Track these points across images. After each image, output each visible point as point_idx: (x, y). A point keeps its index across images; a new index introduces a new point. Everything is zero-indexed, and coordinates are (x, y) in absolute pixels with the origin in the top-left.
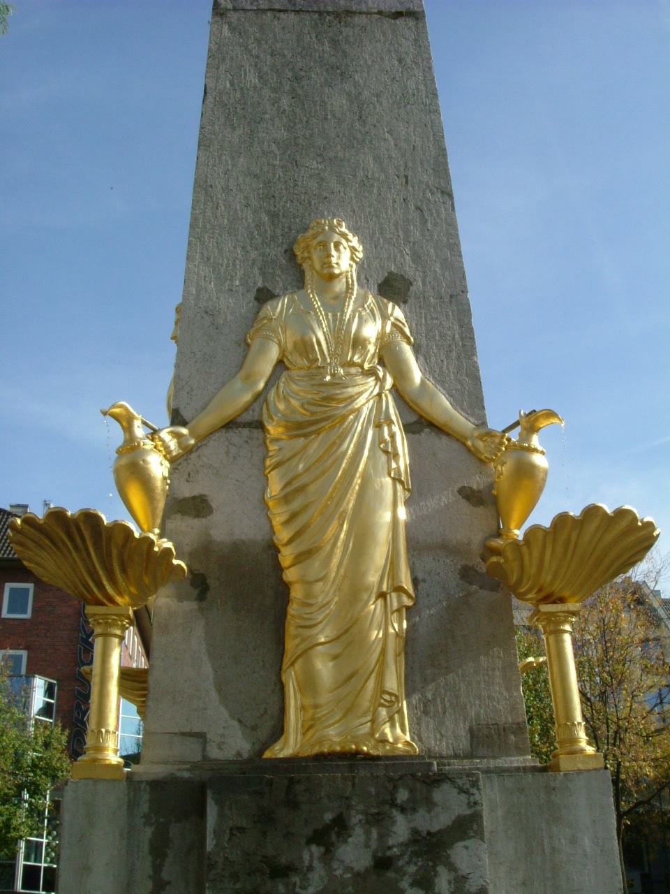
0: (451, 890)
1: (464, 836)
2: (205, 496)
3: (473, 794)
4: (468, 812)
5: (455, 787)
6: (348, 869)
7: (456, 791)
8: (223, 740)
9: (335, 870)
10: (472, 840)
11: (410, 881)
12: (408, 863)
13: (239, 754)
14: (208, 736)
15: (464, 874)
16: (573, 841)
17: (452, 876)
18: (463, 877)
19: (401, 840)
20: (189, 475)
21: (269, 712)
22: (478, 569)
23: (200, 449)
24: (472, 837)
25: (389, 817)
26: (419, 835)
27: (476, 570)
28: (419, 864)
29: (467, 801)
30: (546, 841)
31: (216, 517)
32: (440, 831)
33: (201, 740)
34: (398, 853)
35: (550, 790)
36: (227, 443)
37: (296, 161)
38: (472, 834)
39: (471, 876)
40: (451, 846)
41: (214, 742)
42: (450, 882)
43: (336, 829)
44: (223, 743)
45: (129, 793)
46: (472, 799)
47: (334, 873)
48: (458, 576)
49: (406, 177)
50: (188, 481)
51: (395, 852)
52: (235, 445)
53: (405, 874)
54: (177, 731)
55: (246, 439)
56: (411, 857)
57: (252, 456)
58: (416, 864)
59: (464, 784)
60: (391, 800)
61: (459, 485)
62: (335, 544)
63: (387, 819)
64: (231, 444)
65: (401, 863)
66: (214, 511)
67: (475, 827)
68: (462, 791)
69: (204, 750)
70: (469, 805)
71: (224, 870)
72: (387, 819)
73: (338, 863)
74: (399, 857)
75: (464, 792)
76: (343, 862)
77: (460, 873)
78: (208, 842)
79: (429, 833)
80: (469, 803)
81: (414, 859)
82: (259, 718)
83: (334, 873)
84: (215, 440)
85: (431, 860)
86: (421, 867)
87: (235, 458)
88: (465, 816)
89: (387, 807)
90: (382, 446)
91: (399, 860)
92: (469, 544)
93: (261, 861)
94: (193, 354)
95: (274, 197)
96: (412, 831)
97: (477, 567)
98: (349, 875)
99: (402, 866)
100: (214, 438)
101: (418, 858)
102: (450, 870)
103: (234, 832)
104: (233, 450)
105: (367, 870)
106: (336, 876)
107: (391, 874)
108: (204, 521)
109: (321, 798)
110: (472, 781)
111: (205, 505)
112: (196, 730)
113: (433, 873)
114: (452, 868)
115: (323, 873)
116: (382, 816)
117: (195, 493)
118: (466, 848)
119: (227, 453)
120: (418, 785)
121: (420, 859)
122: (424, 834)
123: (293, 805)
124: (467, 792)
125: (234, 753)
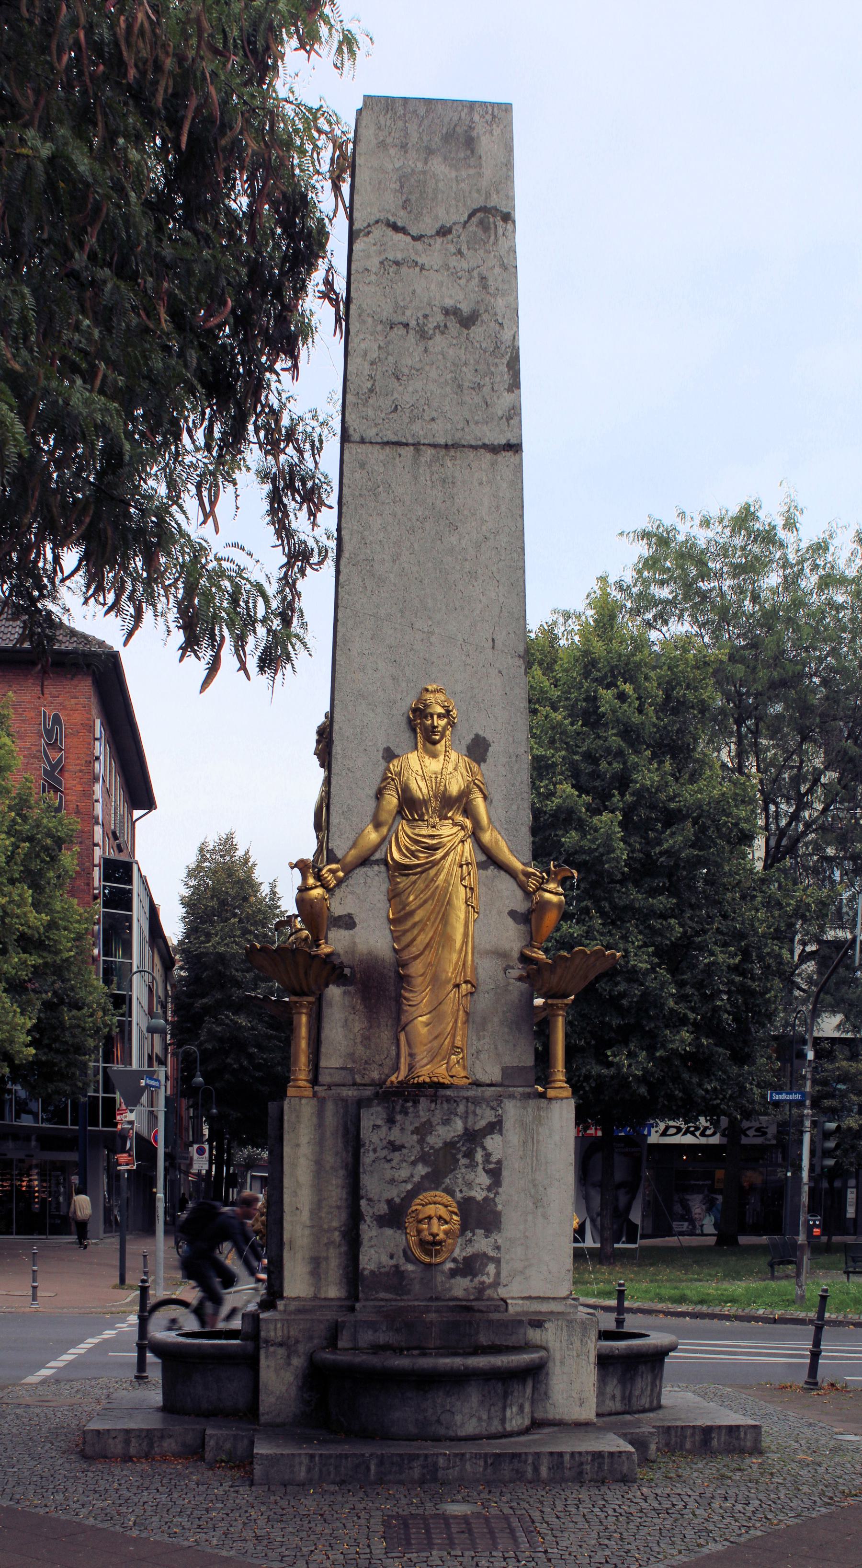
4: (494, 1120)
6: (432, 1148)
35: (539, 1109)
49: (493, 640)
68: (492, 1108)
114: (484, 1149)
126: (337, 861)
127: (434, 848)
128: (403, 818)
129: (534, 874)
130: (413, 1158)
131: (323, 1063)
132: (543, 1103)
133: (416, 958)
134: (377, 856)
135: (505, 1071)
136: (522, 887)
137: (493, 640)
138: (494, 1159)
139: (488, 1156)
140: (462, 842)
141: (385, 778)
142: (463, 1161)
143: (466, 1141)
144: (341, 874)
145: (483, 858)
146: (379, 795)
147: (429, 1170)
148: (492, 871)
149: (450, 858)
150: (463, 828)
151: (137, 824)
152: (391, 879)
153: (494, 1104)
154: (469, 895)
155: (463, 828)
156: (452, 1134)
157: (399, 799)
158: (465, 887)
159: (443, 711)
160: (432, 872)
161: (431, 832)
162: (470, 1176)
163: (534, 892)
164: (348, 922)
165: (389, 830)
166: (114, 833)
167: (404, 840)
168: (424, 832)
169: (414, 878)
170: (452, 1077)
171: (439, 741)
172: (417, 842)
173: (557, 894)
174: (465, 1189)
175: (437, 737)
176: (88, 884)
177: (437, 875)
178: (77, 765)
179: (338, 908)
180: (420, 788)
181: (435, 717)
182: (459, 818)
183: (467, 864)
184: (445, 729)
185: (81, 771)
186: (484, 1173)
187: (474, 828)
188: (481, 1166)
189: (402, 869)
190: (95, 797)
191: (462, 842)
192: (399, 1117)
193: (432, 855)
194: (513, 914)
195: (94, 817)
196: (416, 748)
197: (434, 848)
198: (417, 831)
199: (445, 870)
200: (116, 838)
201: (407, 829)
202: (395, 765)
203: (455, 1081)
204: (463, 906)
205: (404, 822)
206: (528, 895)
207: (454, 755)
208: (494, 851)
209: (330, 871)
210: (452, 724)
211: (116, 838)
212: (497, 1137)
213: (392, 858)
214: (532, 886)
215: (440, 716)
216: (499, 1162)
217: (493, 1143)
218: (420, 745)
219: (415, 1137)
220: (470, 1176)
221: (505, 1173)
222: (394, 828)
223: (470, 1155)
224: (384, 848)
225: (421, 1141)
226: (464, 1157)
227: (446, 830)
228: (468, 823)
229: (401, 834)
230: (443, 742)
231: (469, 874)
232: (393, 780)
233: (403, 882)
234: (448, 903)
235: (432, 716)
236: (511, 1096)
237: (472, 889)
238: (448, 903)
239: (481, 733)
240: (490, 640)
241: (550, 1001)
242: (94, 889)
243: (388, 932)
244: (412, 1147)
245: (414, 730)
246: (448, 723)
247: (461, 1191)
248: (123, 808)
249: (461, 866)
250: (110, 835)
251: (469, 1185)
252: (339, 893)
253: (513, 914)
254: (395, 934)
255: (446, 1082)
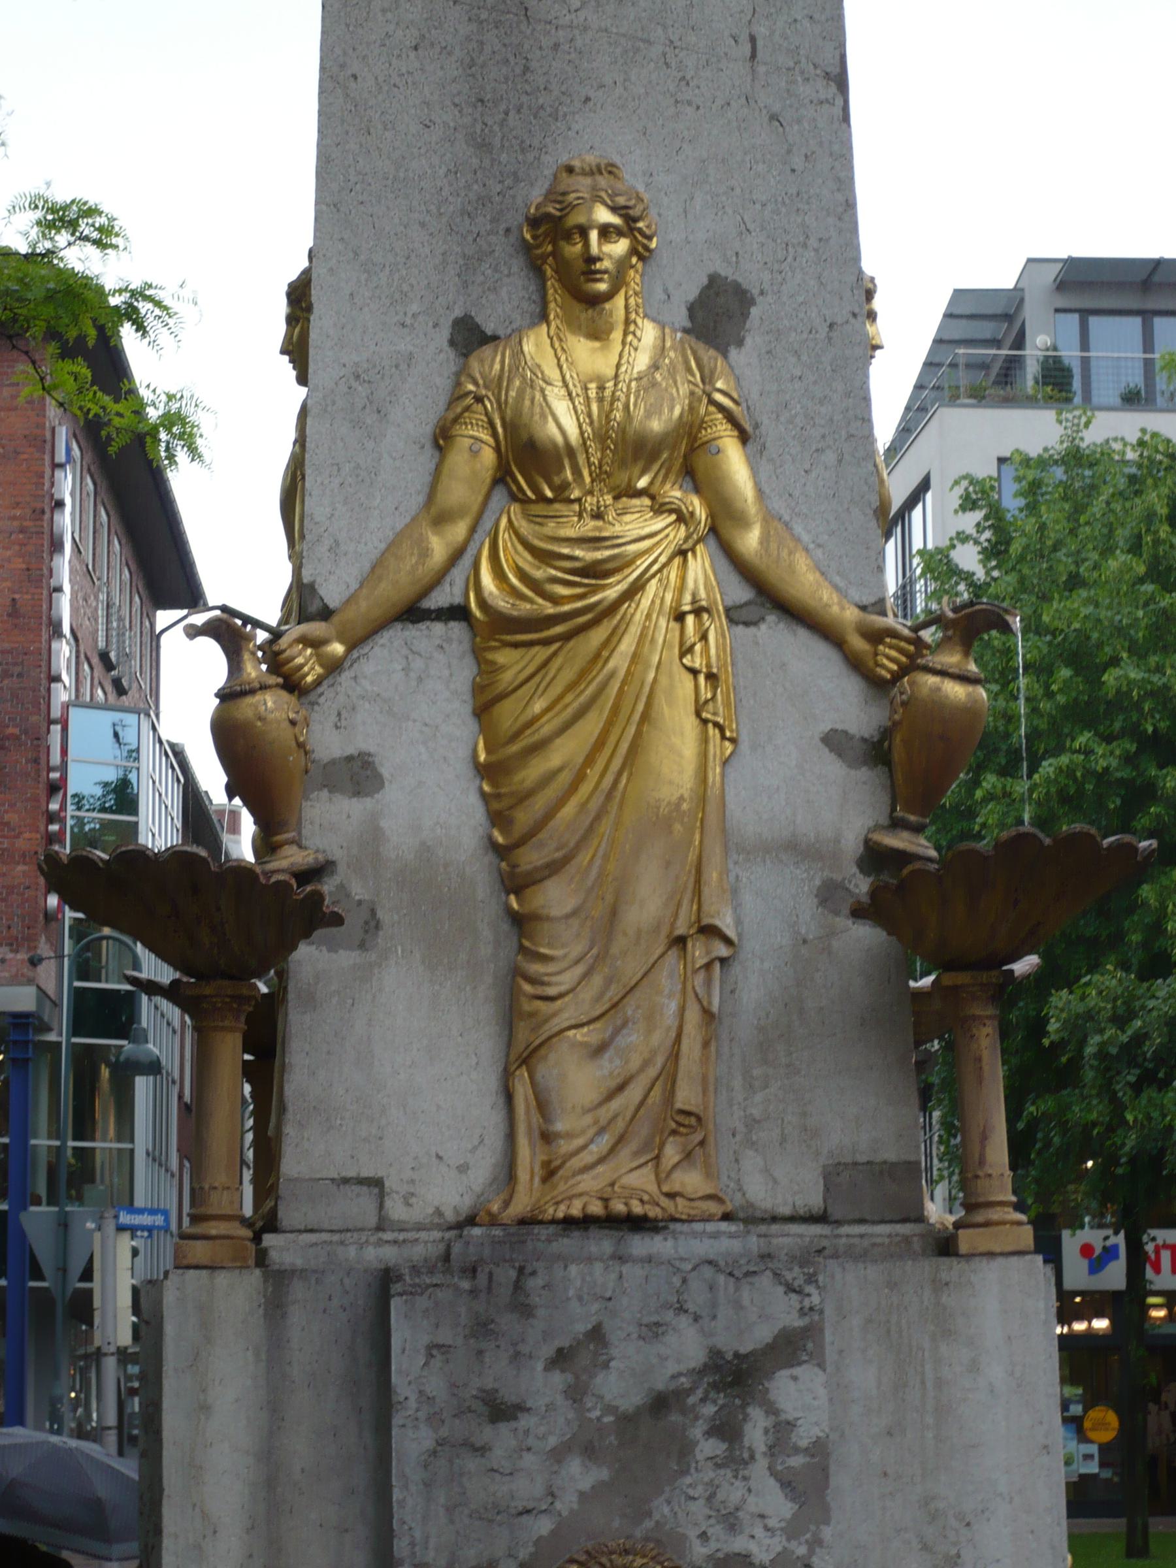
0: (769, 1443)
1: (792, 1361)
2: (369, 755)
3: (809, 1295)
4: (799, 1323)
5: (781, 1283)
6: (610, 1409)
7: (781, 1289)
8: (412, 1190)
9: (589, 1410)
10: (804, 1366)
11: (705, 1428)
12: (703, 1400)
13: (438, 1212)
14: (387, 1184)
15: (790, 1418)
16: (974, 1367)
17: (768, 1422)
18: (788, 1423)
19: (692, 1364)
20: (339, 714)
21: (486, 1141)
22: (851, 887)
23: (356, 665)
24: (805, 1362)
25: (674, 1329)
26: (724, 1358)
27: (847, 889)
28: (720, 1402)
29: (798, 1307)
30: (928, 1367)
31: (393, 795)
32: (752, 1353)
33: (376, 1191)
34: (687, 1386)
35: (939, 1286)
36: (405, 651)
37: (526, 9)
38: (805, 1358)
39: (799, 1422)
40: (770, 1375)
41: (397, 1193)
42: (766, 1431)
43: (592, 1347)
44: (413, 1194)
45: (266, 1290)
46: (807, 1303)
47: (588, 1415)
48: (815, 900)
49: (753, 39)
50: (337, 727)
51: (682, 1384)
52: (420, 655)
53: (697, 1418)
54: (336, 1176)
55: (438, 642)
56: (707, 1392)
57: (451, 675)
58: (714, 1402)
59: (794, 1279)
60: (678, 1302)
61: (826, 727)
62: (637, 698)
63: (671, 1332)
64: (414, 653)
65: (691, 1400)
66: (387, 784)
67: (810, 1346)
68: (790, 1289)
69: (381, 1206)
70: (802, 1312)
71: (417, 1410)
72: (671, 1332)
73: (594, 1399)
74: (690, 1392)
75: (794, 1291)
76: (601, 1397)
77: (783, 1417)
78: (393, 1368)
79: (737, 1355)
80: (801, 1309)
81: (712, 1395)
82: (470, 1152)
83: (588, 1415)
84: (382, 645)
85: (738, 1397)
86: (722, 1408)
87: (420, 680)
88: (795, 1329)
89: (671, 1313)
90: (684, 661)
91: (688, 1396)
92: (837, 841)
93: (475, 1397)
94: (335, 468)
95: (482, 101)
96: (710, 1351)
97: (850, 882)
98: (611, 1419)
99: (694, 1405)
100: (382, 641)
101: (718, 1393)
102: (767, 1412)
103: (435, 1352)
104: (418, 664)
105: (638, 1411)
106: (590, 1420)
107: (675, 1417)
108: (368, 803)
109: (568, 1299)
110: (809, 1274)
111: (369, 772)
112: (365, 1173)
113: (741, 1417)
114: (772, 1410)
115: (571, 1415)
116: (664, 1328)
117: (351, 750)
118: (795, 1378)
119: (406, 670)
120: (721, 1279)
121: (722, 1395)
122: (729, 1356)
123: (525, 1311)
124: (799, 1292)
125: (430, 1211)
126: (326, 614)
127: (596, 572)
128: (514, 498)
129: (893, 634)
130: (552, 1441)
131: (291, 1165)
132: (949, 1268)
133: (554, 868)
134: (439, 599)
135: (831, 1176)
136: (855, 663)
137: (753, 39)
138: (804, 1435)
139: (782, 1429)
140: (682, 553)
141: (457, 396)
142: (710, 1447)
143: (714, 1386)
144: (338, 648)
145: (741, 593)
146: (442, 438)
147: (604, 1474)
148: (774, 633)
149: (646, 600)
150: (682, 518)
151: (164, 639)
152: (478, 654)
153: (795, 1275)
154: (705, 694)
155: (682, 518)
156: (672, 1368)
157: (497, 449)
158: (694, 672)
159: (615, 220)
160: (598, 636)
161: (589, 527)
162: (732, 1493)
163: (897, 677)
164: (359, 775)
165: (473, 530)
166: (104, 657)
167: (512, 554)
168: (570, 532)
169: (541, 653)
170: (671, 1196)
171: (609, 296)
172: (544, 557)
173: (964, 678)
174: (716, 1530)
175: (603, 287)
176: (36, 761)
177: (610, 643)
178: (14, 518)
179: (328, 743)
180: (563, 420)
181: (594, 235)
182: (674, 494)
183: (698, 612)
184: (623, 265)
185: (22, 530)
186: (772, 1482)
187: (712, 515)
188: (762, 1463)
189: (501, 628)
190: (53, 583)
191: (682, 553)
192: (507, 1322)
193: (595, 589)
194: (834, 741)
195: (50, 622)
196: (544, 317)
197: (596, 572)
198: (550, 528)
199: (634, 631)
200: (108, 665)
201: (524, 527)
202: (493, 362)
203: (681, 1207)
204: (690, 724)
205: (515, 508)
206: (878, 685)
207: (648, 333)
208: (775, 575)
209: (306, 641)
210: (640, 252)
211: (108, 665)
212: (805, 1372)
213: (483, 603)
214: (888, 660)
215: (606, 232)
216: (819, 1450)
217: (798, 1393)
218: (553, 310)
219: (558, 1379)
220: (732, 1493)
221: (840, 1480)
222: (487, 524)
223: (727, 1430)
224: (459, 574)
225: (576, 1393)
226: (709, 1434)
227: (639, 529)
228: (698, 507)
229: (504, 536)
230: (619, 301)
231: (704, 637)
232: (479, 399)
233: (512, 663)
234: (645, 717)
235: (583, 232)
236: (859, 1255)
237: (711, 677)
238: (645, 717)
239: (725, 271)
240: (744, 38)
241: (949, 979)
242: (50, 769)
243: (474, 800)
244: (550, 1407)
245: (536, 268)
246: (633, 251)
247: (704, 1536)
248: (127, 602)
249: (680, 617)
250: (95, 660)
251: (731, 1521)
252: (329, 700)
253: (834, 741)
254: (496, 806)
255: (653, 1212)
